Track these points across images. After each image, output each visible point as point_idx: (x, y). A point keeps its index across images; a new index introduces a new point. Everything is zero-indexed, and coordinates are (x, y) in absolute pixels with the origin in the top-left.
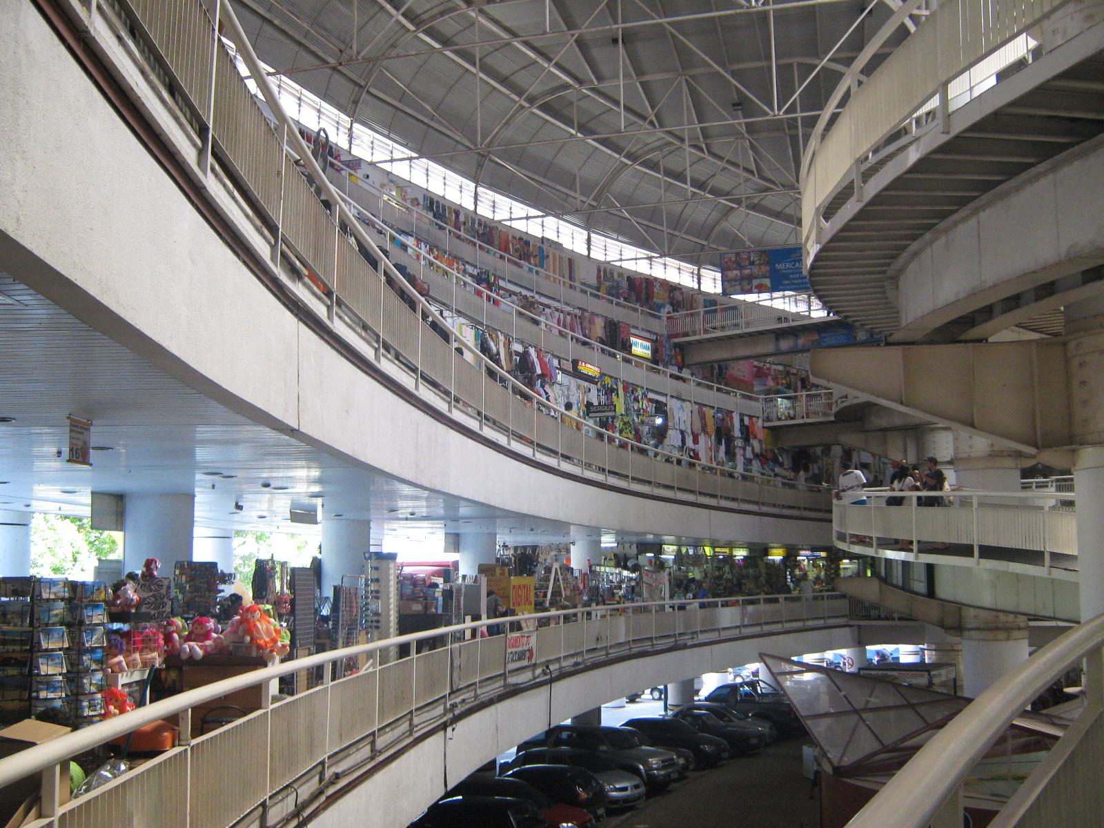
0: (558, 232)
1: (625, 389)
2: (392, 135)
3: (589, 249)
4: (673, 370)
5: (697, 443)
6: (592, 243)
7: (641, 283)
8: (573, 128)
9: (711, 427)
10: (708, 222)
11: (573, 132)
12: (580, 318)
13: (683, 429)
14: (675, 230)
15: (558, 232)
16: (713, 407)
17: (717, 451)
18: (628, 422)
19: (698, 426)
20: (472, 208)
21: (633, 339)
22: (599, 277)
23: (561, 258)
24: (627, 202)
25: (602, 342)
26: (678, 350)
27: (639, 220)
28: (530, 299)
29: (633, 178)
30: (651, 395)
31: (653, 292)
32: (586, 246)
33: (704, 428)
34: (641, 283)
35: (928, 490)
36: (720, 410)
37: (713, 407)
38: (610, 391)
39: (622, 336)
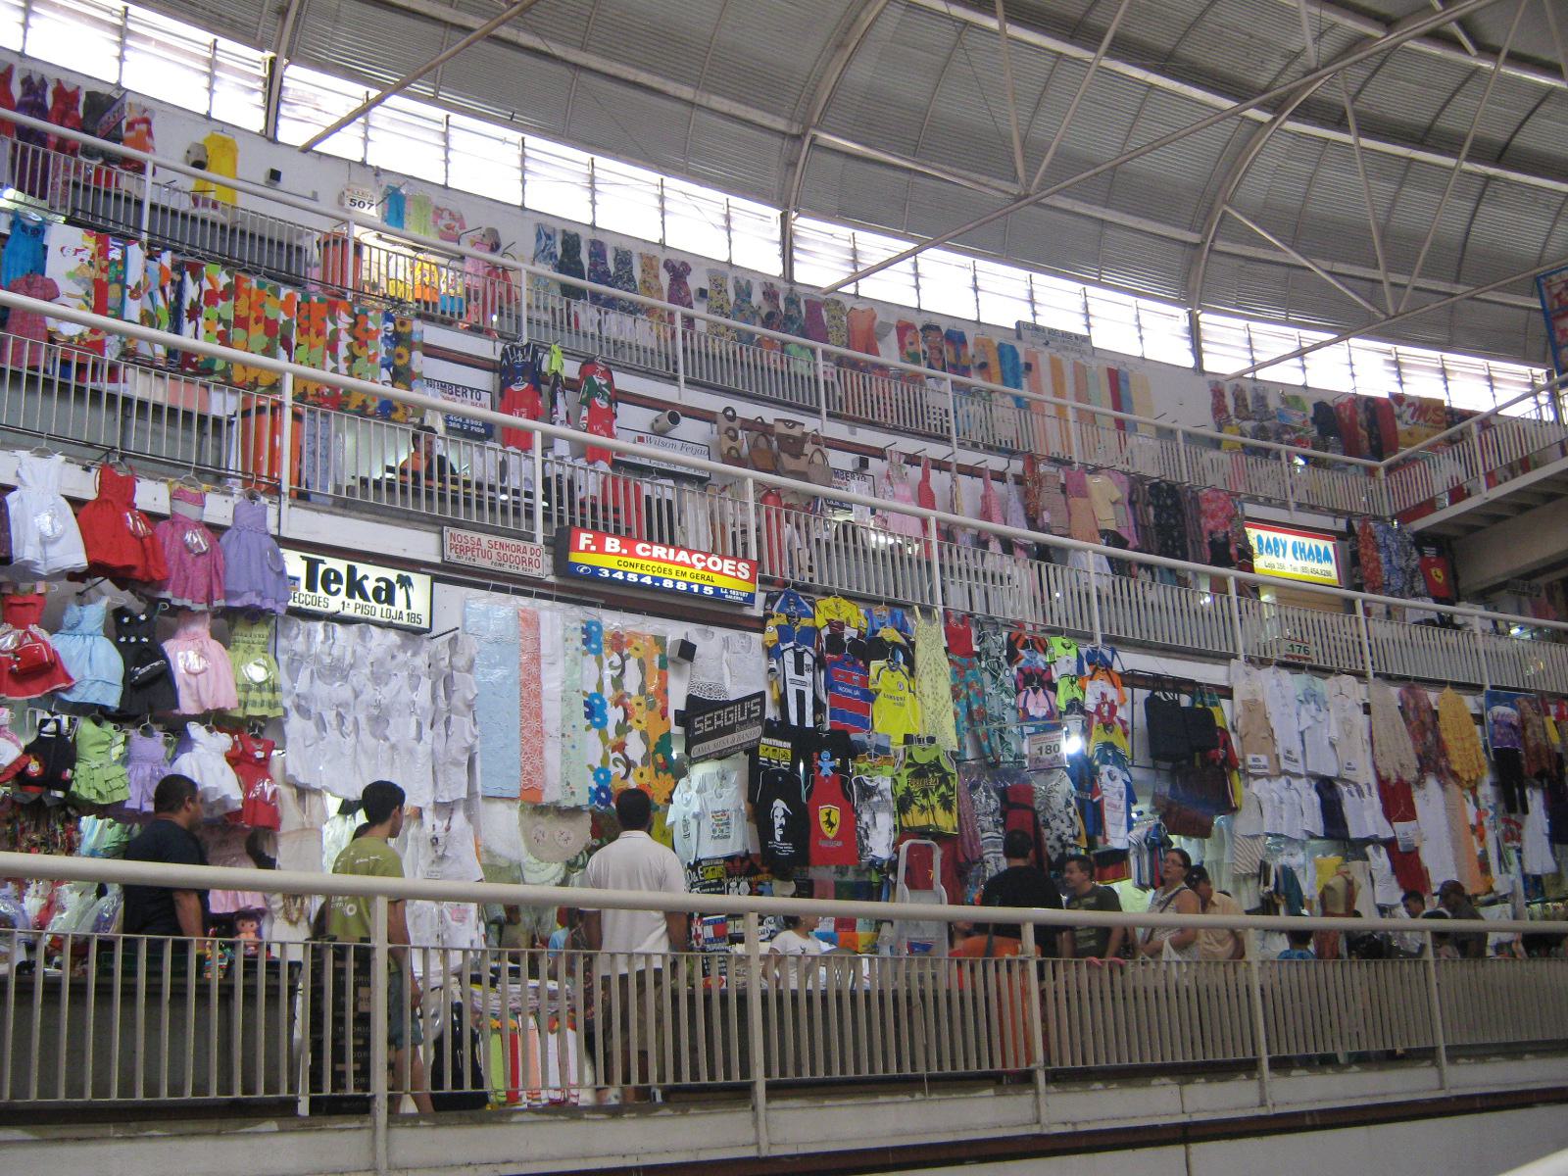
0: (1140, 327)
1: (957, 643)
2: (444, 96)
3: (1197, 352)
4: (1429, 606)
5: (1409, 814)
6: (1204, 336)
7: (1354, 412)
8: (993, 14)
9: (1468, 747)
10: (1551, 251)
11: (993, 24)
12: (1019, 480)
13: (1329, 770)
14: (1457, 281)
15: (1140, 327)
16: (1474, 688)
17: (1513, 833)
18: (936, 766)
19: (1402, 756)
20: (774, 267)
21: (1253, 534)
22: (1219, 409)
23: (1080, 371)
24: (1300, 229)
25: (1116, 539)
26: (1430, 552)
27: (1341, 268)
28: (781, 429)
29: (1288, 158)
30: (1129, 661)
31: (1395, 432)
32: (1188, 345)
33: (1433, 760)
34: (1354, 412)
35: (931, 867)
36: (1499, 695)
37: (1474, 688)
38: (849, 657)
39: (1208, 524)
